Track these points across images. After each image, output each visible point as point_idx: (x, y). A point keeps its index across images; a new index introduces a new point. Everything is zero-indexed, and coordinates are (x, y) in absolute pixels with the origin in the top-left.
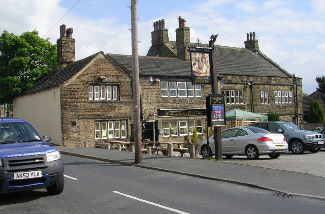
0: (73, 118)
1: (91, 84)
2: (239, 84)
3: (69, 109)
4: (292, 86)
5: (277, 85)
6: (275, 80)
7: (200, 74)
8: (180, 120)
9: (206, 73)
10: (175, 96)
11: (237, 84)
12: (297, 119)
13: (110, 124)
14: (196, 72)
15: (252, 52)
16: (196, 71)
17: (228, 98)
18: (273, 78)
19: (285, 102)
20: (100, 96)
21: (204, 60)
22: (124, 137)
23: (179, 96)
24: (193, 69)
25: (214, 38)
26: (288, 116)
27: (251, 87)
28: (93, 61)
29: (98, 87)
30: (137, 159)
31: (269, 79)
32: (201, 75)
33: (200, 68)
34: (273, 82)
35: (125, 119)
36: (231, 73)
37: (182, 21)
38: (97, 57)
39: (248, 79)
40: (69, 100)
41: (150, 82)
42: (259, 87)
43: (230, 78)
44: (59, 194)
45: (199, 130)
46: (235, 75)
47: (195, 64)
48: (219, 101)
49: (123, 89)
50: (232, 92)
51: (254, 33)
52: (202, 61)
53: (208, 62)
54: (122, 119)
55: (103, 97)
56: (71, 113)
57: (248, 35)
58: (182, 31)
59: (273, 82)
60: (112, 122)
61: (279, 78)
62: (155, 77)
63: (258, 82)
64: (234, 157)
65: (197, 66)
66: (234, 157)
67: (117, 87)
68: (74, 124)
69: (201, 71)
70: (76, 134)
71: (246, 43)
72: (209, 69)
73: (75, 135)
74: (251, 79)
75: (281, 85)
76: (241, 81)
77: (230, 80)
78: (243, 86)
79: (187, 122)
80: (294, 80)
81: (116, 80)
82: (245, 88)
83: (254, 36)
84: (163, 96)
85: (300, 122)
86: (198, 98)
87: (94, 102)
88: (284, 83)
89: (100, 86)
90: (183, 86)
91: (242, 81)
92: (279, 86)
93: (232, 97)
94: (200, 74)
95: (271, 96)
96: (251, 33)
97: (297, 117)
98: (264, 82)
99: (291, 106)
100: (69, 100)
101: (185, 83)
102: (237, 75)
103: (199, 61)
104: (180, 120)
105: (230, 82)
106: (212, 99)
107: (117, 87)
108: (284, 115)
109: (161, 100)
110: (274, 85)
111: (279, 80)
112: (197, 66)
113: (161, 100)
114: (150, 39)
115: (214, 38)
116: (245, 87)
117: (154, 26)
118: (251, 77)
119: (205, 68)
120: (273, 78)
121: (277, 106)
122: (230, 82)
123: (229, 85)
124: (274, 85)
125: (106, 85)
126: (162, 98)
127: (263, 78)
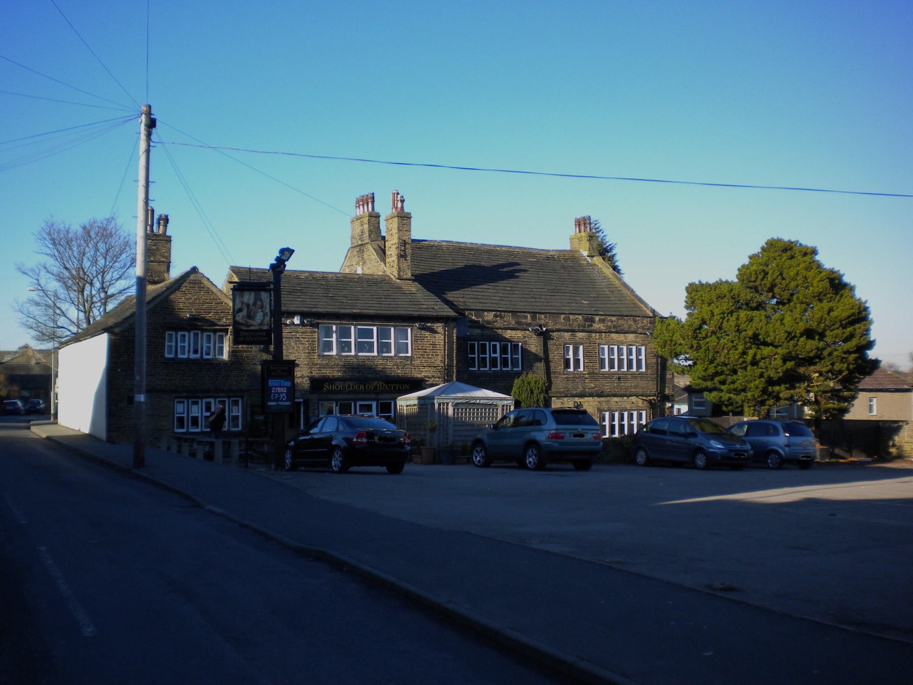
7: (249, 326)
9: (261, 324)
14: (242, 324)
18: (597, 318)
20: (189, 351)
21: (259, 303)
25: (286, 253)
26: (634, 399)
30: (139, 461)
31: (586, 320)
32: (252, 328)
34: (596, 326)
39: (534, 318)
50: (495, 346)
53: (268, 307)
55: (196, 352)
58: (404, 218)
59: (596, 326)
61: (614, 319)
62: (303, 315)
63: (559, 327)
69: (251, 322)
75: (616, 332)
76: (516, 323)
79: (374, 404)
87: (176, 362)
91: (518, 323)
93: (493, 355)
94: (249, 326)
108: (622, 396)
110: (600, 332)
111: (612, 322)
118: (543, 316)
119: (259, 316)
120: (597, 318)
124: (600, 332)
127: (571, 317)
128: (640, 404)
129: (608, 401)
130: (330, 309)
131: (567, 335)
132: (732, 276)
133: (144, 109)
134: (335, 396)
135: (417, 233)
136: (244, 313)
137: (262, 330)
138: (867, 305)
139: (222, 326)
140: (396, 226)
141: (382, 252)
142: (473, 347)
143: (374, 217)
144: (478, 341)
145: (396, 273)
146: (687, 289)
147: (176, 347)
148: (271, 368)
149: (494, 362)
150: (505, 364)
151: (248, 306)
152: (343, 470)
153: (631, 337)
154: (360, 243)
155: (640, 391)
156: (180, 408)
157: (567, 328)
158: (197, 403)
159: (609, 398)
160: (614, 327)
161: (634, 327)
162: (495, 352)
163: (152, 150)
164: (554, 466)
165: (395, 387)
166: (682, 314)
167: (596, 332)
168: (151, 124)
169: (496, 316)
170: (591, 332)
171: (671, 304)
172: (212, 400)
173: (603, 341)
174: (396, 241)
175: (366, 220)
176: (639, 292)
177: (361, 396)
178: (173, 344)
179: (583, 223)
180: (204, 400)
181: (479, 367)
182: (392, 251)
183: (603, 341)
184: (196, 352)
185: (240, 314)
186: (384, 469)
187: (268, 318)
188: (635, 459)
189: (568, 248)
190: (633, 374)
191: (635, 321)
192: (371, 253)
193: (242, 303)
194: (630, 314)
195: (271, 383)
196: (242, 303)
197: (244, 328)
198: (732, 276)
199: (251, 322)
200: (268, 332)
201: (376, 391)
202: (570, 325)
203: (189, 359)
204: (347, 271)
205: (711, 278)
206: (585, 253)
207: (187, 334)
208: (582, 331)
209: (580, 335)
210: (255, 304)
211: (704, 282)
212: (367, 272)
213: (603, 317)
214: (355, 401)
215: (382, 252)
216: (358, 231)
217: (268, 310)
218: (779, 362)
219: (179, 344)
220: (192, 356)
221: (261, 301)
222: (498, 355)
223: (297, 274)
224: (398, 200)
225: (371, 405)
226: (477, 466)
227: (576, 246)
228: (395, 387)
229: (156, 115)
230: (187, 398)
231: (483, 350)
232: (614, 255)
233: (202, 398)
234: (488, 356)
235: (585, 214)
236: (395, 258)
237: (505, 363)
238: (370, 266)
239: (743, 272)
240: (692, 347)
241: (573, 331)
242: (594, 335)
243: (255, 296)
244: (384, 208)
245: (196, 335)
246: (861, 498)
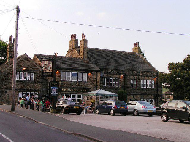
0: (6, 89)
6: (142, 73)
12: (157, 98)
21: (49, 64)
22: (79, 103)
24: (43, 69)
28: (20, 59)
31: (138, 72)
32: (47, 72)
33: (46, 68)
34: (140, 74)
35: (37, 91)
37: (84, 36)
38: (23, 57)
40: (4, 79)
42: (130, 77)
45: (74, 100)
47: (44, 66)
50: (111, 79)
51: (138, 43)
53: (52, 66)
54: (35, 91)
55: (25, 79)
56: (5, 86)
57: (135, 44)
58: (85, 41)
63: (130, 74)
64: (185, 121)
66: (185, 121)
68: (6, 92)
70: (7, 98)
73: (7, 98)
75: (146, 76)
77: (109, 72)
79: (76, 95)
83: (138, 45)
84: (61, 80)
93: (110, 82)
97: (157, 97)
100: (4, 79)
101: (77, 73)
106: (51, 83)
107: (33, 73)
108: (147, 95)
112: (45, 67)
115: (55, 54)
117: (71, 37)
119: (49, 68)
120: (141, 72)
126: (61, 81)
127: (133, 72)
128: (152, 97)
131: (132, 77)
132: (182, 61)
133: (16, 7)
134: (65, 93)
135: (90, 45)
136: (45, 67)
138: (165, 73)
139: (33, 71)
140: (83, 43)
141: (79, 52)
142: (105, 79)
143: (76, 41)
144: (106, 78)
145: (83, 57)
146: (168, 64)
147: (20, 77)
149: (111, 84)
150: (113, 85)
151: (46, 65)
152: (114, 115)
153: (150, 78)
154: (72, 48)
155: (153, 93)
156: (20, 95)
158: (25, 93)
160: (146, 75)
161: (151, 75)
162: (111, 81)
163: (19, 19)
164: (154, 116)
165: (82, 91)
166: (167, 72)
168: (18, 11)
169: (111, 71)
171: (163, 68)
172: (29, 93)
173: (142, 79)
174: (83, 48)
175: (74, 41)
176: (153, 65)
177: (72, 93)
178: (19, 76)
179: (137, 44)
180: (27, 93)
181: (106, 85)
182: (82, 51)
183: (142, 79)
186: (76, 114)
187: (52, 69)
188: (110, 113)
189: (132, 51)
190: (151, 89)
191: (152, 73)
192: (75, 51)
193: (45, 64)
194: (151, 72)
195: (52, 88)
196: (45, 64)
198: (182, 61)
200: (52, 73)
201: (76, 92)
203: (23, 80)
204: (68, 56)
205: (175, 62)
206: (137, 53)
207: (23, 73)
209: (136, 77)
210: (48, 65)
212: (74, 56)
214: (71, 94)
215: (79, 52)
216: (71, 44)
217: (52, 67)
219: (20, 76)
220: (24, 80)
222: (112, 82)
223: (33, 58)
224: (84, 36)
225: (75, 96)
226: (112, 115)
227: (134, 51)
228: (82, 91)
229: (20, 8)
230: (22, 92)
231: (108, 80)
232: (144, 53)
233: (27, 92)
234: (109, 82)
235: (137, 42)
236: (82, 53)
237: (107, 84)
238: (76, 55)
239: (185, 60)
240: (170, 80)
244: (79, 38)
245: (25, 73)
246: (92, 125)
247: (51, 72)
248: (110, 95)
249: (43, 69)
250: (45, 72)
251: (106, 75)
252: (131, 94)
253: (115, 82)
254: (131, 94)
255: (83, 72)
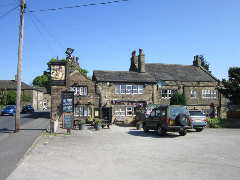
1: (71, 86)
2: (175, 86)
3: (56, 99)
4: (217, 87)
5: (205, 87)
7: (57, 78)
8: (127, 107)
9: (61, 78)
10: (124, 93)
11: (173, 86)
13: (81, 108)
14: (54, 78)
15: (196, 67)
16: (53, 77)
17: (167, 94)
18: (201, 82)
19: (208, 97)
21: (61, 70)
23: (126, 93)
24: (52, 76)
27: (183, 88)
29: (75, 88)
32: (58, 79)
33: (57, 75)
34: (201, 85)
36: (173, 80)
37: (141, 51)
39: (181, 83)
40: (56, 95)
41: (107, 85)
43: (167, 82)
44: (184, 135)
46: (171, 81)
47: (53, 73)
48: (69, 96)
49: (90, 89)
52: (59, 70)
56: (57, 102)
59: (201, 85)
60: (83, 107)
61: (206, 82)
62: (110, 82)
65: (55, 73)
67: (86, 88)
69: (57, 77)
71: (193, 62)
72: (64, 76)
74: (184, 83)
75: (207, 86)
76: (176, 84)
77: (167, 84)
78: (177, 87)
80: (218, 84)
81: (85, 84)
82: (179, 89)
84: (115, 93)
85: (224, 110)
86: (140, 94)
88: (210, 85)
89: (76, 87)
90: (130, 88)
92: (206, 87)
94: (57, 78)
95: (199, 94)
96: (196, 56)
97: (220, 107)
98: (194, 85)
99: (216, 99)
100: (56, 95)
101: (132, 86)
102: (173, 81)
103: (56, 71)
104: (127, 107)
105: (167, 85)
107: (86, 88)
109: (114, 95)
110: (202, 87)
111: (206, 83)
112: (55, 73)
113: (114, 95)
114: (130, 62)
116: (179, 88)
119: (61, 75)
121: (204, 99)
122: (167, 85)
123: (167, 87)
124: (202, 87)
125: (80, 87)
127: (193, 82)
129: (205, 107)
130: (118, 80)
137: (62, 80)
148: (65, 94)
157: (192, 85)
159: (205, 106)
161: (213, 85)
167: (201, 87)
169: (169, 82)
170: (199, 86)
184: (78, 93)
185: (53, 74)
197: (54, 79)
199: (57, 77)
202: (193, 85)
208: (196, 86)
211: (237, 67)
213: (203, 82)
218: (57, 135)
221: (62, 69)
235: (197, 55)
241: (194, 86)
242: (200, 87)
243: (59, 67)
245: (78, 88)
247: (63, 79)
248: (171, 132)
249: (52, 76)
250: (56, 80)
251: (165, 87)
252: (192, 105)
253: (138, 89)
254: (192, 105)
255: (138, 84)
